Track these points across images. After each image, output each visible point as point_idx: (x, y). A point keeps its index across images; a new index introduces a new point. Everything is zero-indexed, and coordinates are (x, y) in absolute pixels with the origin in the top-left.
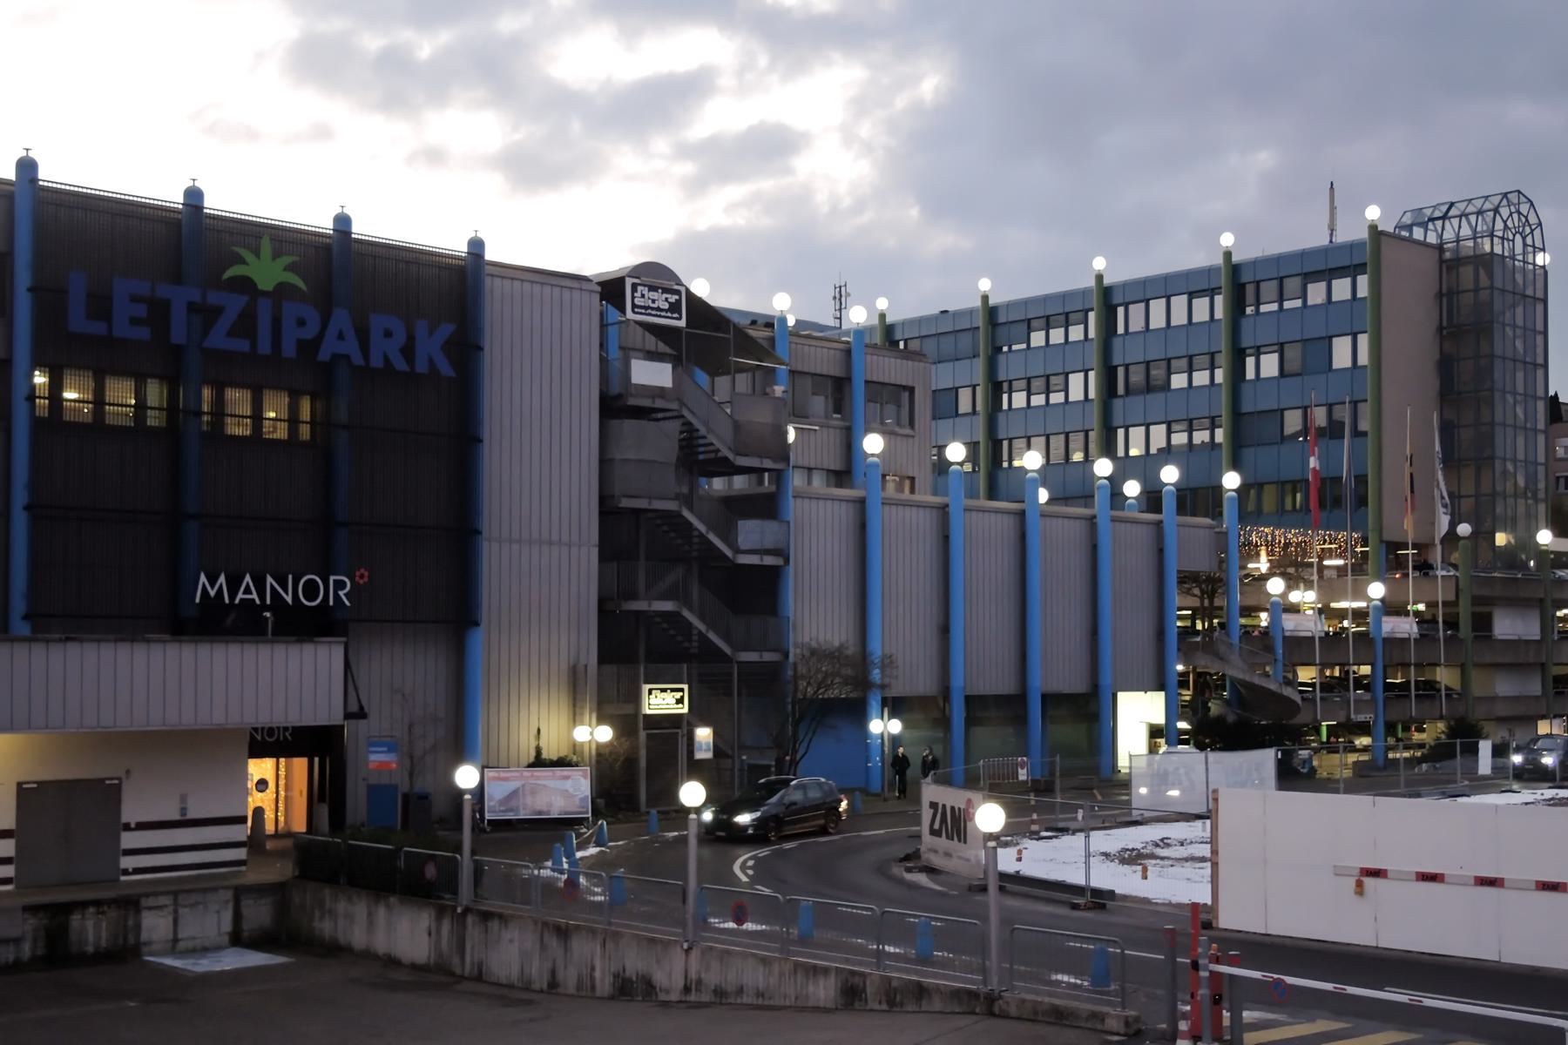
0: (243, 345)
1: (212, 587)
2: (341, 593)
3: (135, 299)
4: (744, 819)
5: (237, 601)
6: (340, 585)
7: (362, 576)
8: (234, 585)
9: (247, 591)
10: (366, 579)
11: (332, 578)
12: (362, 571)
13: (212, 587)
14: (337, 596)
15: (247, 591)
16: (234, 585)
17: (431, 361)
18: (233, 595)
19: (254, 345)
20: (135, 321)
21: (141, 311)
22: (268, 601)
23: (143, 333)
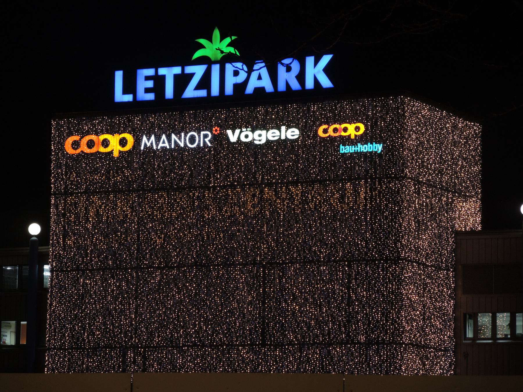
0: (203, 93)
1: (148, 142)
2: (207, 140)
3: (147, 78)
4: (424, 204)
5: (159, 148)
6: (206, 136)
7: (216, 130)
8: (158, 139)
9: (164, 142)
10: (218, 132)
11: (202, 133)
12: (216, 128)
13: (148, 142)
14: (204, 142)
15: (164, 142)
16: (158, 139)
17: (316, 80)
18: (157, 145)
19: (209, 92)
20: (147, 90)
21: (150, 84)
22: (173, 147)
23: (151, 97)
